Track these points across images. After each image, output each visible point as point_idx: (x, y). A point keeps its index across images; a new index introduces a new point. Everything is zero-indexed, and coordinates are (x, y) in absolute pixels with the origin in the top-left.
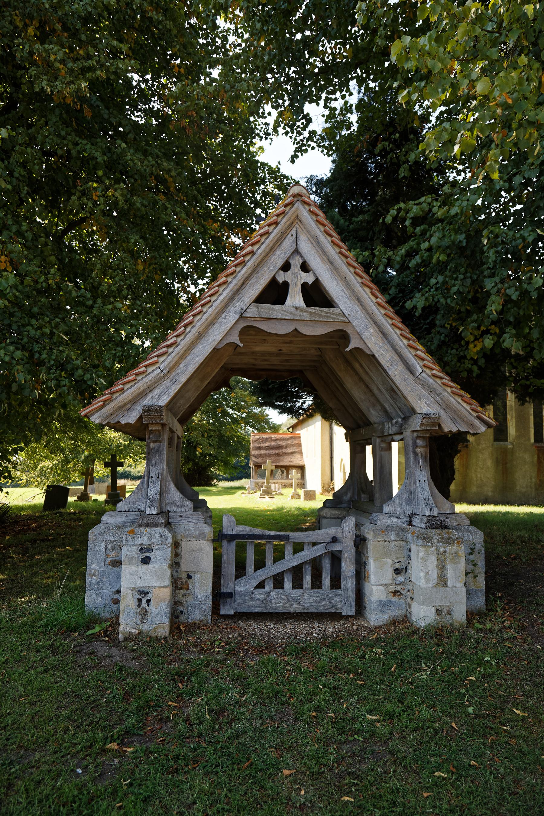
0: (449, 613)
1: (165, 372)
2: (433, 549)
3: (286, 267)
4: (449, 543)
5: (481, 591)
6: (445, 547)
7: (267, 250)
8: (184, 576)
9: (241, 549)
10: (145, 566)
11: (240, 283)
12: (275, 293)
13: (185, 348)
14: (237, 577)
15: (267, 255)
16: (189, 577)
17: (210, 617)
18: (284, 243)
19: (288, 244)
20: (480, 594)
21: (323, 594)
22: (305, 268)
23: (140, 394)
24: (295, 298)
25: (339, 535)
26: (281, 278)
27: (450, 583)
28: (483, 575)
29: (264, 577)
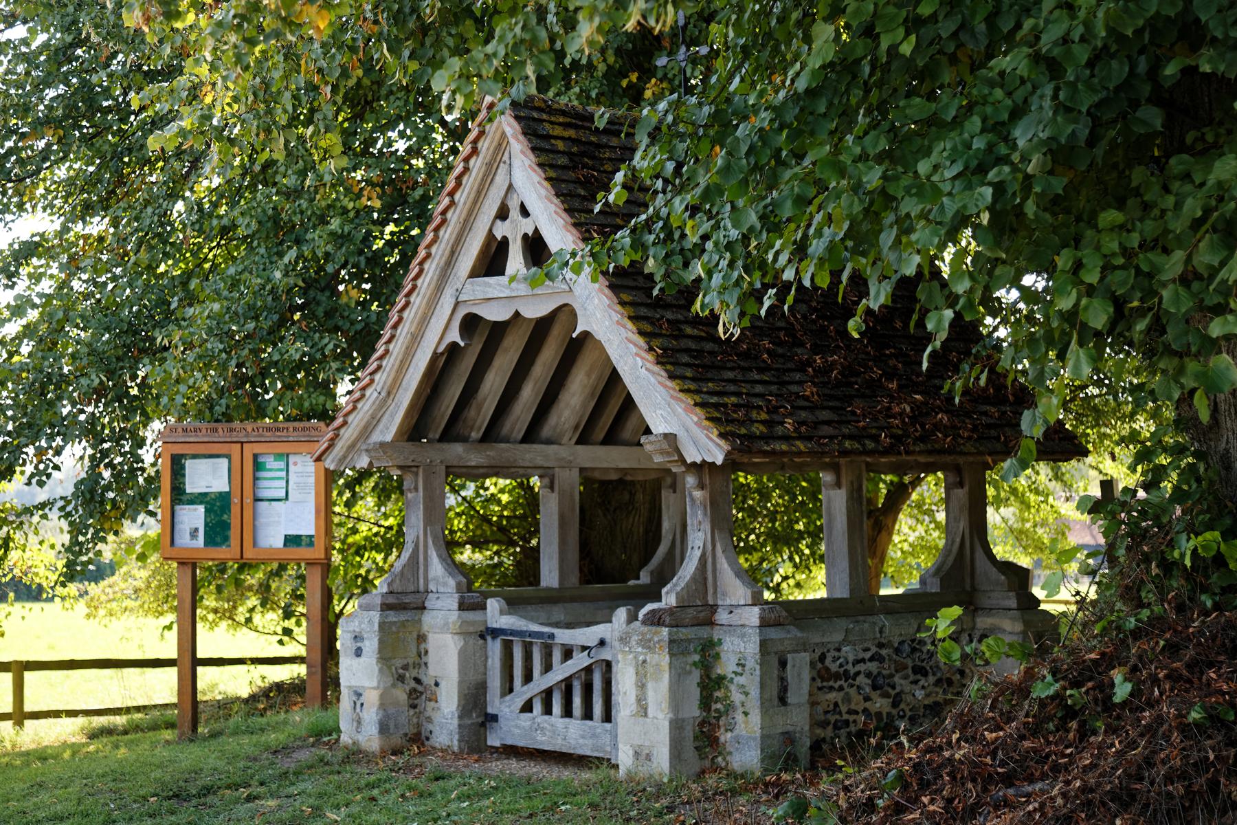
0: (648, 757)
1: (383, 394)
2: (631, 656)
3: (503, 214)
4: (649, 648)
5: (755, 739)
6: (646, 654)
7: (473, 195)
8: (433, 683)
9: (508, 648)
10: (358, 660)
11: (447, 252)
12: (492, 260)
13: (400, 357)
14: (503, 695)
15: (475, 202)
16: (437, 684)
17: (456, 743)
18: (497, 178)
19: (501, 181)
20: (753, 744)
21: (590, 728)
22: (525, 212)
23: (366, 427)
24: (516, 261)
25: (608, 637)
26: (501, 230)
27: (650, 714)
28: (757, 711)
29: (528, 696)
